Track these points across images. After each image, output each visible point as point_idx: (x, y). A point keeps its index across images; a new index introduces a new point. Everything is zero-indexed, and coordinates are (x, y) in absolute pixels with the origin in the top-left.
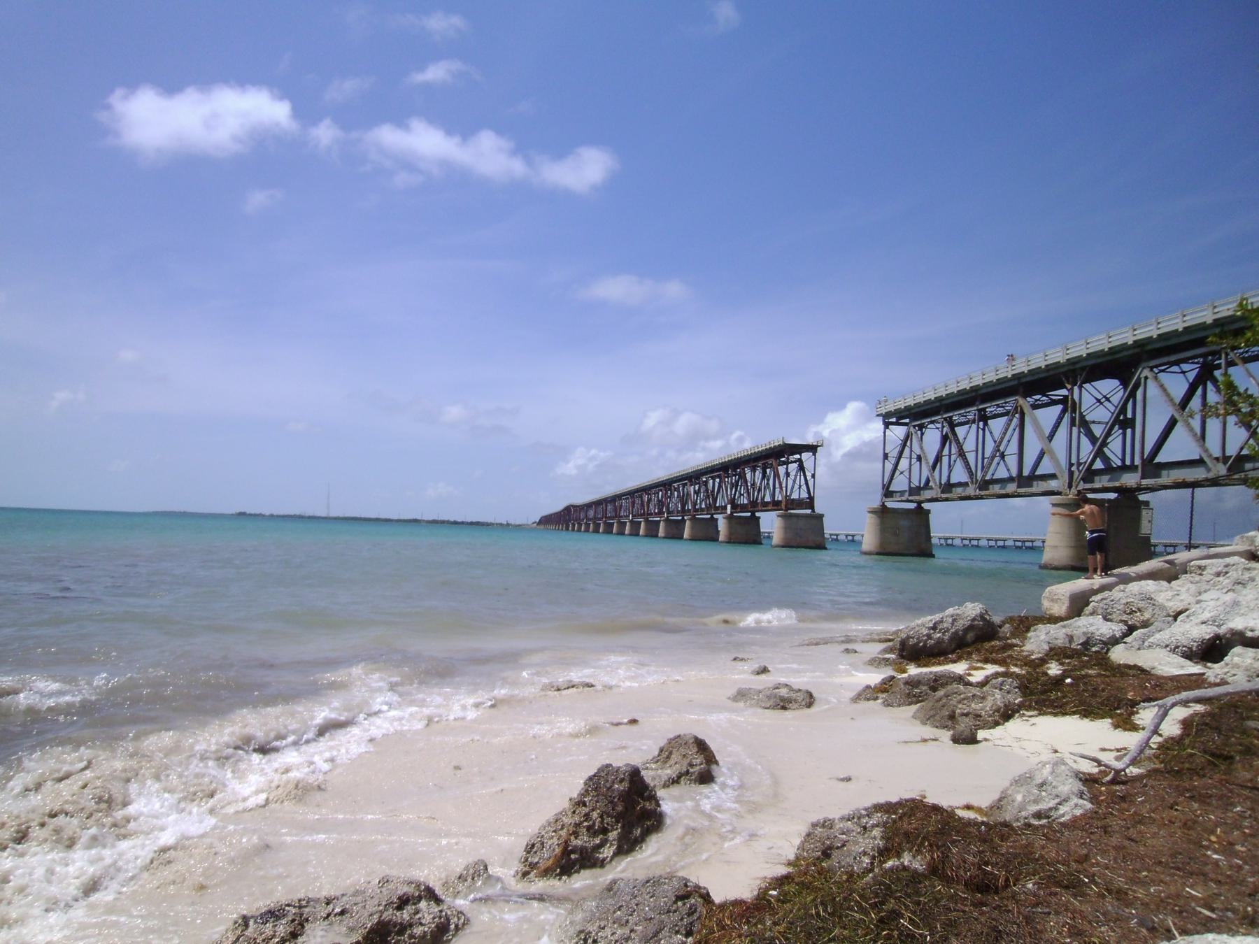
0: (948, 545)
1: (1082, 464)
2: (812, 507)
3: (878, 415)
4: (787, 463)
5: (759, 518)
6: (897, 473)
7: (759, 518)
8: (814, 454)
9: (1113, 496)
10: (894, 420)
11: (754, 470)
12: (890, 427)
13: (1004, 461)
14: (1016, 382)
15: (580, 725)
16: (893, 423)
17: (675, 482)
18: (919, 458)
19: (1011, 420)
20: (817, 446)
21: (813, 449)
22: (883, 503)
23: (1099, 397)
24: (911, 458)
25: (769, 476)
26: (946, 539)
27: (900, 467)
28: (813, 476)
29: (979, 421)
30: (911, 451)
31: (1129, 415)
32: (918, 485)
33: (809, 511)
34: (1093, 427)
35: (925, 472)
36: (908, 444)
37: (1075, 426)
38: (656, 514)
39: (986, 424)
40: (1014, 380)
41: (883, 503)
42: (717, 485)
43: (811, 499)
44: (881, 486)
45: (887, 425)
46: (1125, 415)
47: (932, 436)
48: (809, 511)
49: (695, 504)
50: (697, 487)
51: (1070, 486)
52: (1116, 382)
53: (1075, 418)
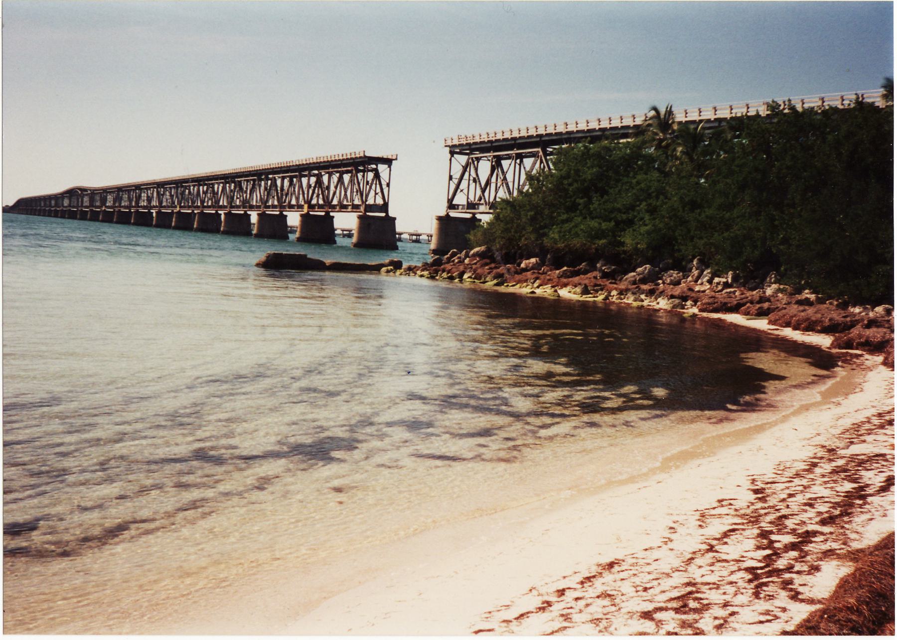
2: (386, 211)
4: (310, 176)
5: (333, 217)
6: (459, 190)
7: (333, 217)
8: (390, 167)
11: (330, 175)
12: (455, 155)
15: (497, 448)
18: (475, 181)
21: (388, 162)
24: (469, 180)
25: (295, 185)
27: (461, 187)
28: (388, 185)
30: (470, 175)
33: (383, 215)
35: (479, 192)
36: (468, 170)
39: (521, 161)
44: (446, 201)
45: (452, 153)
47: (485, 167)
48: (383, 215)
49: (202, 202)
50: (205, 188)
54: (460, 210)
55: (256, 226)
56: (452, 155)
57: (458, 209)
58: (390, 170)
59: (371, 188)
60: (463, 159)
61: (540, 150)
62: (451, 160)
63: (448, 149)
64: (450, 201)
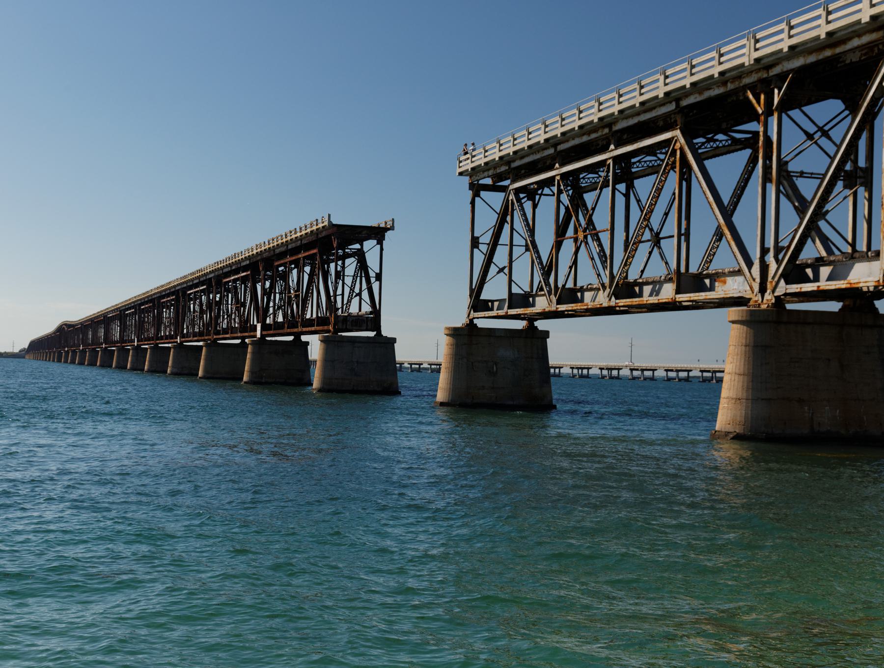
0: (611, 377)
1: (783, 248)
3: (461, 174)
6: (493, 270)
8: (380, 242)
9: (834, 306)
10: (488, 181)
12: (483, 194)
13: (660, 248)
14: (551, 151)
16: (487, 188)
17: (191, 288)
19: (662, 182)
20: (386, 229)
21: (378, 233)
22: (471, 321)
23: (811, 129)
26: (610, 369)
28: (379, 277)
29: (617, 181)
31: (862, 163)
32: (527, 289)
33: (371, 334)
34: (800, 183)
36: (509, 218)
37: (771, 181)
38: (195, 334)
39: (630, 187)
40: (603, 127)
41: (471, 321)
42: (306, 277)
43: (376, 312)
45: (476, 189)
46: (855, 162)
48: (371, 334)
50: (268, 284)
51: (763, 290)
52: (375, 242)
53: (771, 167)
54: (494, 313)
55: (318, 364)
56: (476, 194)
57: (492, 309)
58: (382, 249)
59: (352, 289)
60: (496, 199)
61: (677, 133)
62: (473, 203)
63: (466, 180)
64: (476, 292)
